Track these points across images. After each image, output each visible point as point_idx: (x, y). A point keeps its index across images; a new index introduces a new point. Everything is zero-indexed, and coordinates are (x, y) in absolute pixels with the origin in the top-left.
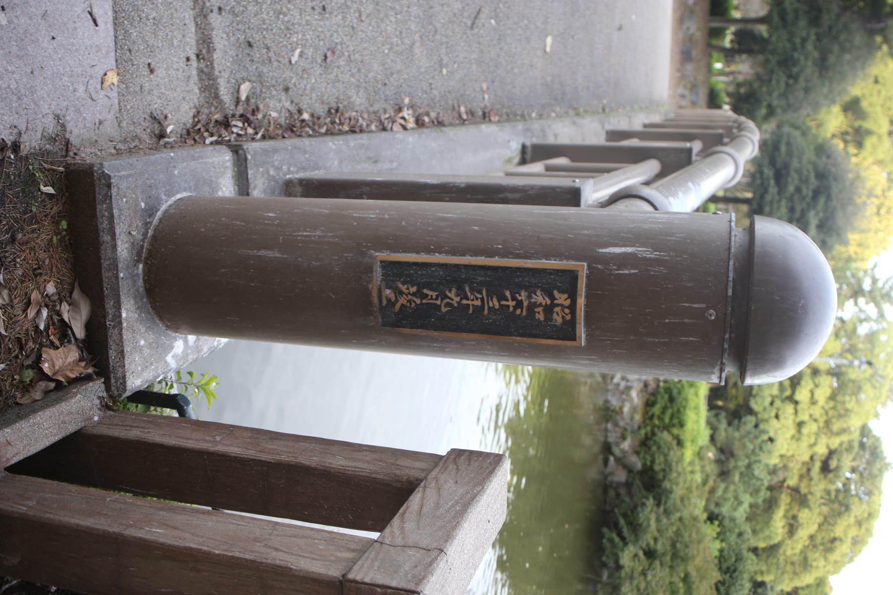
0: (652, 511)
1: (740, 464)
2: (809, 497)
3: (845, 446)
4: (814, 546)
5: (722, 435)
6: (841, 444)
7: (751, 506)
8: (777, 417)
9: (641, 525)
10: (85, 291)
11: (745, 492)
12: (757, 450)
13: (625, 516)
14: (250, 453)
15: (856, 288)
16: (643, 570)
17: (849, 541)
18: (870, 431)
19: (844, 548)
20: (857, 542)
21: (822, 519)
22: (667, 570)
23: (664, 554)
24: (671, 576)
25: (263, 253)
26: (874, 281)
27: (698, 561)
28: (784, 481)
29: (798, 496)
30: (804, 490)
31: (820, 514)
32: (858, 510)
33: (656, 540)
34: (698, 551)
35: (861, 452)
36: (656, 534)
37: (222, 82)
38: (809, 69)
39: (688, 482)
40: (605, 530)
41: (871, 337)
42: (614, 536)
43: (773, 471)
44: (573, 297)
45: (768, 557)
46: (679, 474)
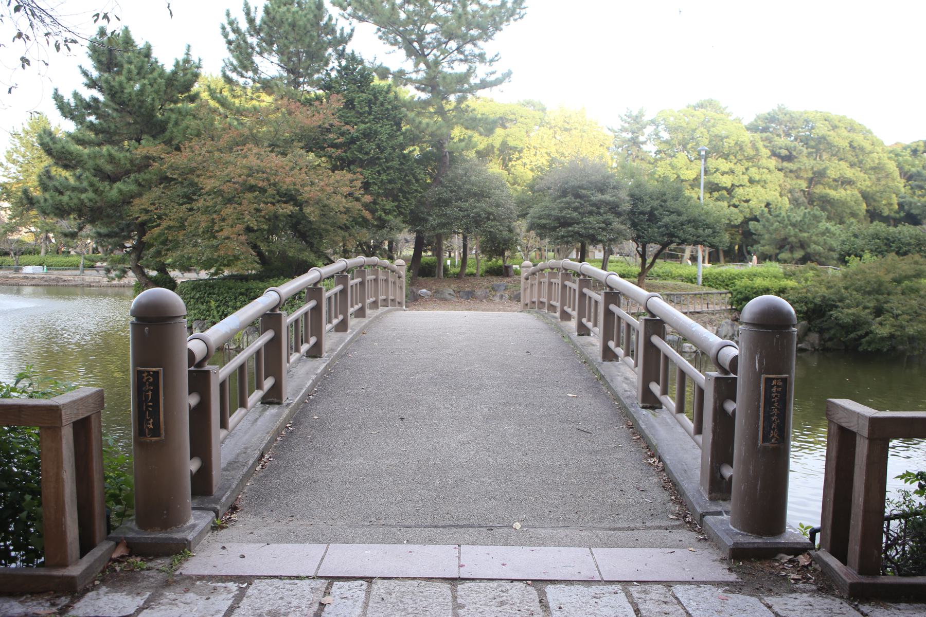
0: (842, 313)
1: (792, 233)
2: (815, 169)
3: (766, 143)
4: (861, 162)
5: (768, 249)
6: (766, 147)
7: (829, 219)
8: (747, 201)
9: (854, 321)
10: (776, 555)
11: (817, 227)
12: (779, 219)
13: (847, 333)
14: (833, 486)
15: (631, 143)
16: (893, 318)
17: (851, 135)
18: (751, 124)
19: (859, 139)
20: (852, 129)
21: (833, 158)
22: (891, 297)
23: (878, 300)
24: (896, 294)
25: (758, 488)
26: (623, 130)
27: (881, 273)
28: (803, 191)
29: (816, 179)
30: (810, 175)
31: (830, 160)
32: (822, 129)
33: (865, 308)
34: (872, 273)
35: (771, 129)
36: (861, 307)
37: (672, 524)
38: (483, 205)
39: (815, 283)
40: (860, 349)
41: (670, 129)
42: (864, 340)
43: (795, 202)
44: (773, 379)
45: (875, 200)
46: (808, 291)
